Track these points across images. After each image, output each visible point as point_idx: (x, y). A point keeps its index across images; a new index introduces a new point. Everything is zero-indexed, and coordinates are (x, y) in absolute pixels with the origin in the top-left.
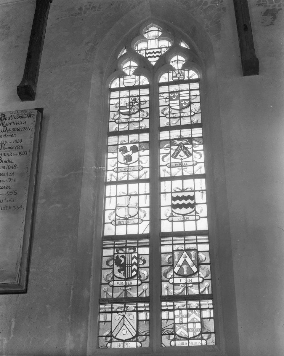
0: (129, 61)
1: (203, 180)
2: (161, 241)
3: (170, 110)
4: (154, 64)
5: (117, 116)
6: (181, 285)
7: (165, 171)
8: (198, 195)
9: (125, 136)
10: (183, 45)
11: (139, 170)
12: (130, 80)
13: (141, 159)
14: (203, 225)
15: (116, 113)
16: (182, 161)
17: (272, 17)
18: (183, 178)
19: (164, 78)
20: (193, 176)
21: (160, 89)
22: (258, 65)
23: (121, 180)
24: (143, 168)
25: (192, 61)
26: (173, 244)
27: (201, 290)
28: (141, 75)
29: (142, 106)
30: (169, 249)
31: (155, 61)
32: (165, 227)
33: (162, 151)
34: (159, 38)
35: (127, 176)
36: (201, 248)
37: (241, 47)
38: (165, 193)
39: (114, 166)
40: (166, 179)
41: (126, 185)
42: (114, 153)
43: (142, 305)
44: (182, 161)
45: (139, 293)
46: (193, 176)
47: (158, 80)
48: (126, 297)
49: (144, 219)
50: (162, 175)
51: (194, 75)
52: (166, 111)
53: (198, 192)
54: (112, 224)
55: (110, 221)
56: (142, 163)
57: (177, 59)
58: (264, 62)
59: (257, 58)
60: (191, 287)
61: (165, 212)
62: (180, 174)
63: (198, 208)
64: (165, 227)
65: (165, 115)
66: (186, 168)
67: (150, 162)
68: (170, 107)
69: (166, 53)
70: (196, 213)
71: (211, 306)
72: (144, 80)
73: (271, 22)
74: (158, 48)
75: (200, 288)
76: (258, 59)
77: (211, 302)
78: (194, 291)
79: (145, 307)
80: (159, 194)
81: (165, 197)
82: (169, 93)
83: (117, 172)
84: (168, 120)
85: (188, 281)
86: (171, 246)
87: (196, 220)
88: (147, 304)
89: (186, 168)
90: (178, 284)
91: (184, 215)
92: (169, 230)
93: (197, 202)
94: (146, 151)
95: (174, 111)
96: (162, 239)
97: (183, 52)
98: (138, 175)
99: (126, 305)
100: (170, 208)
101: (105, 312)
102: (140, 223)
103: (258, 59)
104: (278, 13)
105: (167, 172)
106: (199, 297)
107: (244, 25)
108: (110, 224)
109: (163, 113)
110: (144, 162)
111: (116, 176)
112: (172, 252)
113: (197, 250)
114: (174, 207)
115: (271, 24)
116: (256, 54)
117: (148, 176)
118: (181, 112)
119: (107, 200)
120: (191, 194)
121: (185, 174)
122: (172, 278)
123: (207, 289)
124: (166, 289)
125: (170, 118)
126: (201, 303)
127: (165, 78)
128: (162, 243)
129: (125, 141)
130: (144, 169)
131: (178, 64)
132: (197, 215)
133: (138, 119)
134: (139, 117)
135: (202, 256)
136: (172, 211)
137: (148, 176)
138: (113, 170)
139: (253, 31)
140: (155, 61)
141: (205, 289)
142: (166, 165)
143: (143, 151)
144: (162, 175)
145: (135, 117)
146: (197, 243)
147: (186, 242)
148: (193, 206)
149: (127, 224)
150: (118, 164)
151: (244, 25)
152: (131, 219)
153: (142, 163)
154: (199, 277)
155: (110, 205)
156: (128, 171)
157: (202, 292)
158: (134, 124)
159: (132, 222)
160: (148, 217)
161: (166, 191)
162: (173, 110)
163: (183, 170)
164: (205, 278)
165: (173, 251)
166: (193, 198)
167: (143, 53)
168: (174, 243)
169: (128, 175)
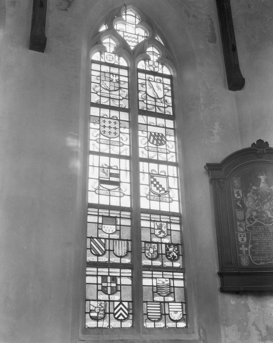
2: (88, 212)
4: (132, 48)
7: (94, 145)
8: (123, 174)
9: (115, 112)
10: (158, 38)
12: (110, 57)
13: (121, 135)
15: (98, 85)
17: (68, 3)
20: (119, 157)
21: (92, 65)
22: (45, 44)
23: (104, 152)
25: (167, 57)
28: (120, 56)
29: (121, 86)
31: (134, 46)
32: (144, 204)
36: (124, 222)
37: (33, 21)
40: (125, 157)
42: (96, 124)
46: (119, 157)
47: (136, 65)
51: (166, 71)
52: (98, 89)
53: (172, 178)
55: (94, 190)
56: (168, 147)
58: (52, 42)
59: (46, 37)
61: (144, 190)
62: (107, 152)
63: (122, 186)
64: (144, 204)
65: (96, 92)
68: (101, 86)
69: (143, 43)
72: (123, 62)
73: (65, 8)
74: (135, 34)
76: (46, 38)
80: (179, 177)
83: (100, 143)
84: (98, 98)
91: (109, 190)
93: (122, 180)
96: (89, 210)
97: (156, 44)
98: (119, 151)
100: (97, 182)
103: (46, 38)
104: (74, 2)
105: (145, 155)
107: (41, 2)
108: (94, 193)
109: (94, 89)
110: (124, 138)
114: (101, 182)
115: (65, 10)
116: (46, 33)
120: (116, 172)
121: (112, 152)
125: (100, 96)
126: (110, 270)
129: (106, 115)
130: (171, 153)
131: (120, 152)
133: (118, 97)
134: (119, 95)
139: (47, 9)
140: (134, 46)
143: (124, 129)
148: (118, 184)
149: (110, 196)
150: (100, 135)
151: (41, 2)
153: (122, 139)
156: (110, 145)
158: (114, 100)
159: (165, 200)
166: (118, 176)
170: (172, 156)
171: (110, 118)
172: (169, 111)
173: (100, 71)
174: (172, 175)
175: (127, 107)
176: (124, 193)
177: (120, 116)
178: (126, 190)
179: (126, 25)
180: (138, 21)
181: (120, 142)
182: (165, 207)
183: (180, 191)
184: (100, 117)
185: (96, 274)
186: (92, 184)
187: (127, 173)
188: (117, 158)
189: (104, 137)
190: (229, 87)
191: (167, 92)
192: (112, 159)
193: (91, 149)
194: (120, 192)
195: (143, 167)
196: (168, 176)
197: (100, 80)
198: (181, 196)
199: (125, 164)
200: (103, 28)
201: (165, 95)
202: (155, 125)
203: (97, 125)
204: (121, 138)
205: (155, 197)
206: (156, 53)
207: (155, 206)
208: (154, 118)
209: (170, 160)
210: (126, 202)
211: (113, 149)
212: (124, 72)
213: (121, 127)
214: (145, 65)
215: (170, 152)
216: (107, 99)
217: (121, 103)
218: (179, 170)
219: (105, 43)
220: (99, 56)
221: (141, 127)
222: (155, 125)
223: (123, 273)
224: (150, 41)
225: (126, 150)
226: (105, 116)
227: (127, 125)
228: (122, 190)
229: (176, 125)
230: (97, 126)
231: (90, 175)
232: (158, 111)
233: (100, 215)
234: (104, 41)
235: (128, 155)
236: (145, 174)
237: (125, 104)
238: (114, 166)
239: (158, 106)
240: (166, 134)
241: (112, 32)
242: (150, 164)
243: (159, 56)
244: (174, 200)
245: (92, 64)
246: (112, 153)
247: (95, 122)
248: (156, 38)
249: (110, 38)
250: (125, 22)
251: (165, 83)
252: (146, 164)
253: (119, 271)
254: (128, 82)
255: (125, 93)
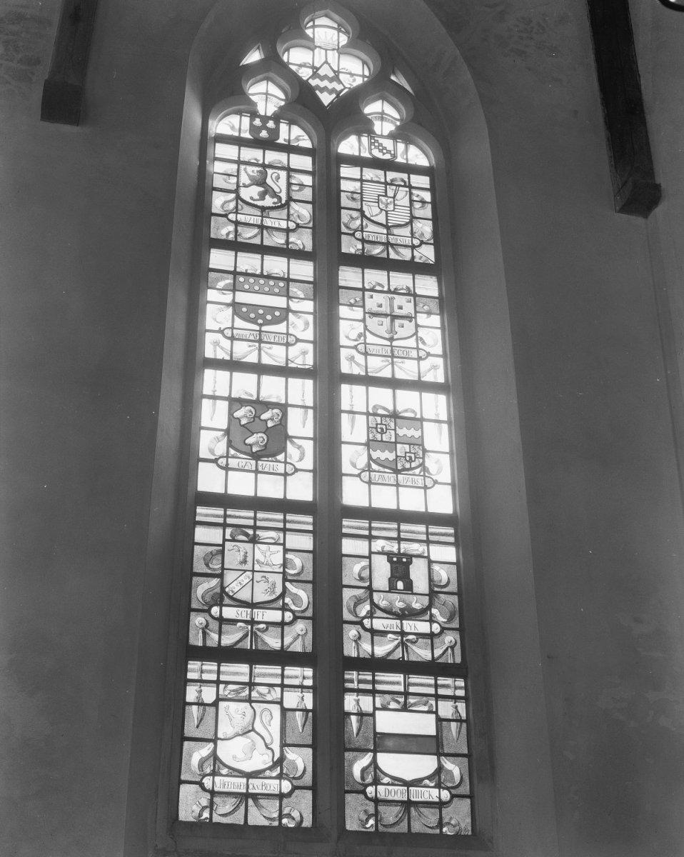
0: (381, 101)
1: (309, 384)
3: (364, 224)
5: (358, 222)
6: (390, 635)
7: (352, 359)
9: (406, 276)
11: (288, 345)
13: (421, 333)
14: (442, 501)
15: (355, 214)
16: (260, 329)
18: (260, 369)
19: (349, 146)
20: (285, 371)
24: (298, 340)
26: (370, 538)
27: (438, 652)
30: (214, 535)
33: (212, 295)
34: (310, 45)
35: (390, 366)
36: (294, 541)
38: (214, 398)
39: (356, 340)
40: (352, 379)
41: (255, 376)
43: (449, 681)
44: (260, 329)
45: (435, 651)
46: (285, 371)
48: (254, 648)
49: (299, 466)
50: (209, 353)
51: (417, 156)
54: (361, 480)
55: (357, 472)
56: (424, 343)
57: (267, 91)
60: (264, 631)
61: (352, 457)
64: (353, 493)
66: (270, 348)
67: (339, 331)
68: (363, 215)
70: (425, 469)
71: (309, 682)
75: (435, 646)
77: (309, 672)
78: (422, 653)
79: (456, 688)
81: (353, 421)
82: (239, 162)
85: (407, 629)
86: (220, 531)
87: (425, 488)
88: (461, 683)
89: (270, 348)
90: (233, 622)
92: (218, 489)
94: (433, 317)
95: (371, 227)
97: (396, 94)
99: (409, 678)
101: (201, 681)
102: (429, 488)
105: (358, 364)
106: (283, 658)
111: (364, 364)
112: (221, 543)
113: (428, 557)
117: (309, 361)
118: (264, 215)
119: (206, 404)
121: (266, 360)
122: (368, 618)
123: (449, 650)
124: (355, 641)
127: (233, 128)
128: (198, 518)
129: (380, 285)
132: (428, 477)
133: (283, 225)
135: (297, 561)
136: (370, 457)
137: (309, 361)
138: (355, 347)
141: (295, 639)
142: (221, 331)
144: (209, 353)
145: (277, 220)
146: (428, 542)
147: (288, 526)
149: (398, 485)
152: (410, 475)
154: (432, 620)
155: (440, 443)
156: (260, 341)
157: (289, 647)
160: (308, 463)
161: (217, 394)
162: (370, 225)
163: (395, 366)
164: (447, 626)
165: (371, 553)
167: (305, 74)
168: (257, 525)
169: (260, 350)
170: (435, 367)
171: (389, 291)
172: (427, 254)
173: (361, 180)
174: (433, 417)
175: (309, 248)
176: (434, 478)
177: (416, 286)
178: (439, 471)
179: (313, 50)
180: (344, 39)
181: (418, 349)
182: (411, 501)
183: (455, 457)
184: (363, 290)
185: (215, 679)
186: (209, 442)
187: (306, 413)
188: (389, 387)
189: (375, 338)
190: (42, 114)
191: (298, 191)
192: (266, 379)
193: (345, 368)
194: (424, 476)
195: (437, 407)
196: (422, 420)
197: (362, 201)
198: (458, 469)
199: (302, 391)
200: (254, 57)
201: (413, 218)
202: (386, 289)
203: (356, 311)
204: (421, 339)
205: (386, 475)
206: (390, 116)
207: (384, 499)
208: (428, 278)
209: (428, 378)
210: (302, 489)
211: (269, 351)
212: (305, 162)
213: (293, 298)
214: (360, 146)
215: (429, 354)
216: (256, 231)
217: (291, 240)
218: (451, 401)
219: (253, 95)
220: (356, 144)
221: (344, 296)
222: (386, 289)
223: (429, 686)
224: (377, 86)
225: (304, 353)
226: (378, 288)
227: (434, 306)
228: (429, 472)
229: (444, 288)
230: (358, 313)
231: (346, 434)
232: (393, 256)
233: (402, 537)
234: (252, 91)
235: (441, 379)
236: (218, 402)
237: (303, 240)
238: (406, 411)
239: (392, 245)
240: (417, 310)
241: (274, 67)
242: (371, 389)
243: (398, 123)
244: (439, 481)
245: (217, 145)
246: (267, 363)
247: (352, 301)
248: (393, 78)
249: (384, 99)
250: (310, 45)
251: (413, 185)
252: (359, 390)
253: (216, 668)
254: (313, 187)
255: (303, 212)
